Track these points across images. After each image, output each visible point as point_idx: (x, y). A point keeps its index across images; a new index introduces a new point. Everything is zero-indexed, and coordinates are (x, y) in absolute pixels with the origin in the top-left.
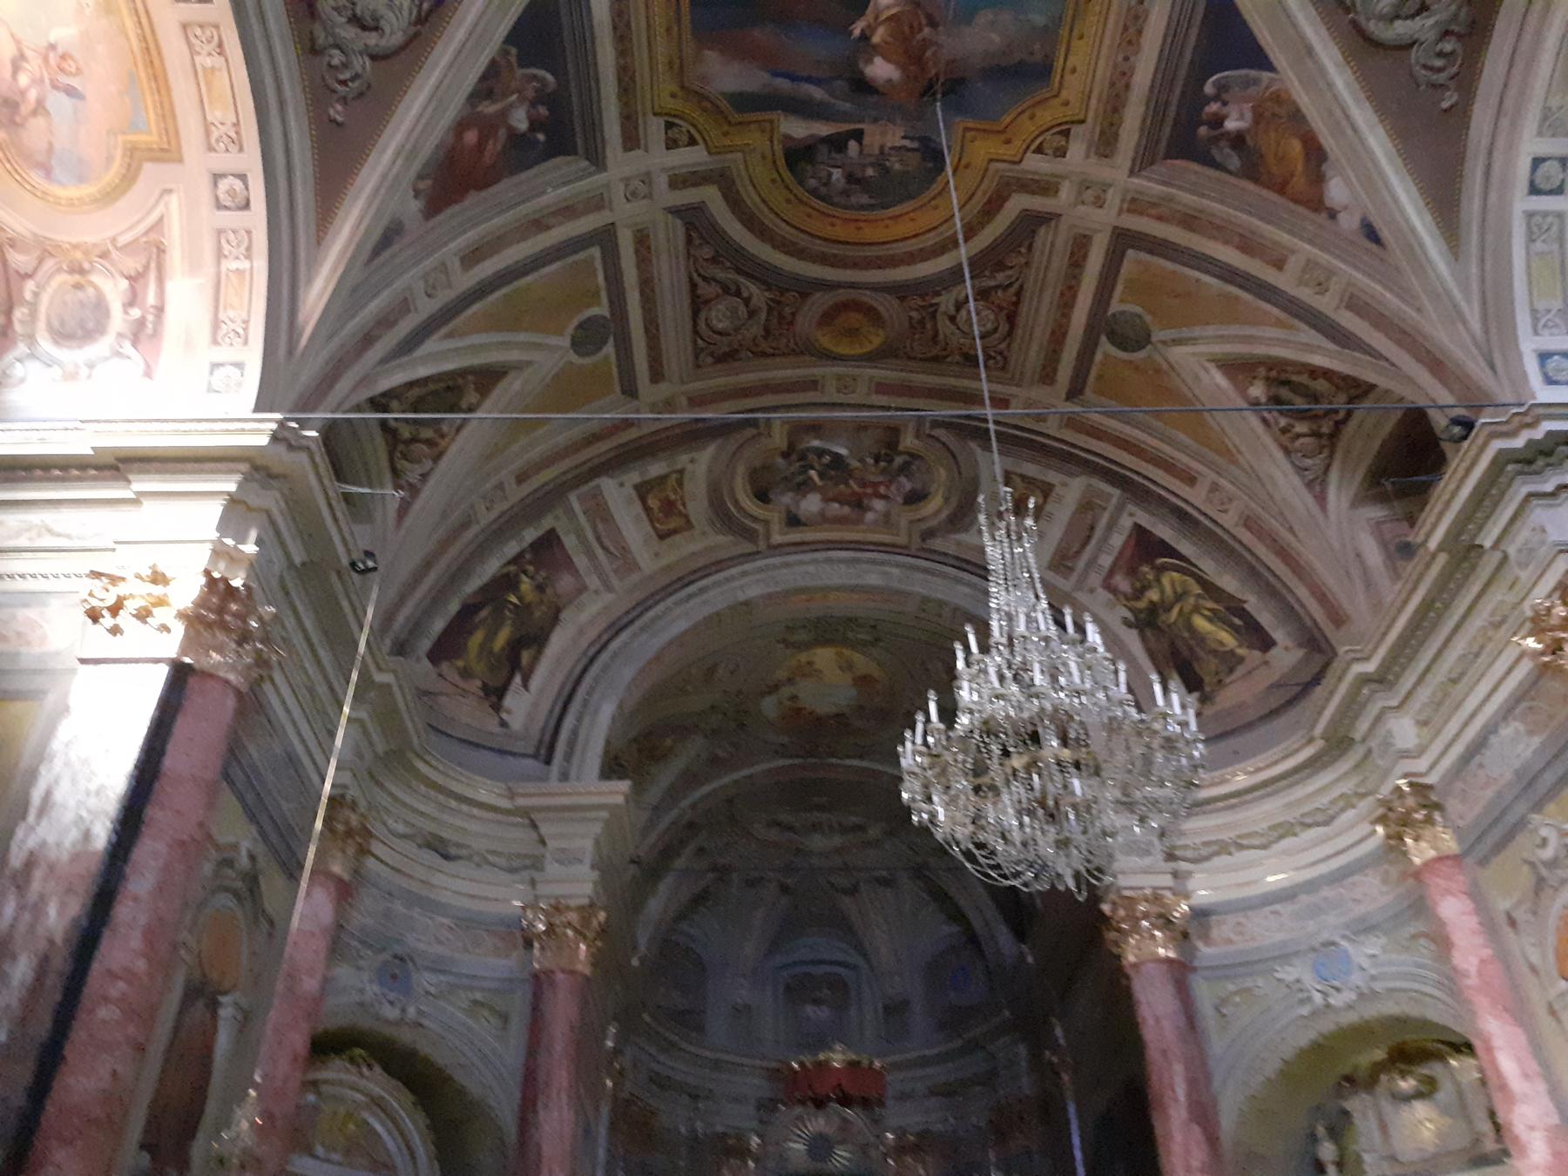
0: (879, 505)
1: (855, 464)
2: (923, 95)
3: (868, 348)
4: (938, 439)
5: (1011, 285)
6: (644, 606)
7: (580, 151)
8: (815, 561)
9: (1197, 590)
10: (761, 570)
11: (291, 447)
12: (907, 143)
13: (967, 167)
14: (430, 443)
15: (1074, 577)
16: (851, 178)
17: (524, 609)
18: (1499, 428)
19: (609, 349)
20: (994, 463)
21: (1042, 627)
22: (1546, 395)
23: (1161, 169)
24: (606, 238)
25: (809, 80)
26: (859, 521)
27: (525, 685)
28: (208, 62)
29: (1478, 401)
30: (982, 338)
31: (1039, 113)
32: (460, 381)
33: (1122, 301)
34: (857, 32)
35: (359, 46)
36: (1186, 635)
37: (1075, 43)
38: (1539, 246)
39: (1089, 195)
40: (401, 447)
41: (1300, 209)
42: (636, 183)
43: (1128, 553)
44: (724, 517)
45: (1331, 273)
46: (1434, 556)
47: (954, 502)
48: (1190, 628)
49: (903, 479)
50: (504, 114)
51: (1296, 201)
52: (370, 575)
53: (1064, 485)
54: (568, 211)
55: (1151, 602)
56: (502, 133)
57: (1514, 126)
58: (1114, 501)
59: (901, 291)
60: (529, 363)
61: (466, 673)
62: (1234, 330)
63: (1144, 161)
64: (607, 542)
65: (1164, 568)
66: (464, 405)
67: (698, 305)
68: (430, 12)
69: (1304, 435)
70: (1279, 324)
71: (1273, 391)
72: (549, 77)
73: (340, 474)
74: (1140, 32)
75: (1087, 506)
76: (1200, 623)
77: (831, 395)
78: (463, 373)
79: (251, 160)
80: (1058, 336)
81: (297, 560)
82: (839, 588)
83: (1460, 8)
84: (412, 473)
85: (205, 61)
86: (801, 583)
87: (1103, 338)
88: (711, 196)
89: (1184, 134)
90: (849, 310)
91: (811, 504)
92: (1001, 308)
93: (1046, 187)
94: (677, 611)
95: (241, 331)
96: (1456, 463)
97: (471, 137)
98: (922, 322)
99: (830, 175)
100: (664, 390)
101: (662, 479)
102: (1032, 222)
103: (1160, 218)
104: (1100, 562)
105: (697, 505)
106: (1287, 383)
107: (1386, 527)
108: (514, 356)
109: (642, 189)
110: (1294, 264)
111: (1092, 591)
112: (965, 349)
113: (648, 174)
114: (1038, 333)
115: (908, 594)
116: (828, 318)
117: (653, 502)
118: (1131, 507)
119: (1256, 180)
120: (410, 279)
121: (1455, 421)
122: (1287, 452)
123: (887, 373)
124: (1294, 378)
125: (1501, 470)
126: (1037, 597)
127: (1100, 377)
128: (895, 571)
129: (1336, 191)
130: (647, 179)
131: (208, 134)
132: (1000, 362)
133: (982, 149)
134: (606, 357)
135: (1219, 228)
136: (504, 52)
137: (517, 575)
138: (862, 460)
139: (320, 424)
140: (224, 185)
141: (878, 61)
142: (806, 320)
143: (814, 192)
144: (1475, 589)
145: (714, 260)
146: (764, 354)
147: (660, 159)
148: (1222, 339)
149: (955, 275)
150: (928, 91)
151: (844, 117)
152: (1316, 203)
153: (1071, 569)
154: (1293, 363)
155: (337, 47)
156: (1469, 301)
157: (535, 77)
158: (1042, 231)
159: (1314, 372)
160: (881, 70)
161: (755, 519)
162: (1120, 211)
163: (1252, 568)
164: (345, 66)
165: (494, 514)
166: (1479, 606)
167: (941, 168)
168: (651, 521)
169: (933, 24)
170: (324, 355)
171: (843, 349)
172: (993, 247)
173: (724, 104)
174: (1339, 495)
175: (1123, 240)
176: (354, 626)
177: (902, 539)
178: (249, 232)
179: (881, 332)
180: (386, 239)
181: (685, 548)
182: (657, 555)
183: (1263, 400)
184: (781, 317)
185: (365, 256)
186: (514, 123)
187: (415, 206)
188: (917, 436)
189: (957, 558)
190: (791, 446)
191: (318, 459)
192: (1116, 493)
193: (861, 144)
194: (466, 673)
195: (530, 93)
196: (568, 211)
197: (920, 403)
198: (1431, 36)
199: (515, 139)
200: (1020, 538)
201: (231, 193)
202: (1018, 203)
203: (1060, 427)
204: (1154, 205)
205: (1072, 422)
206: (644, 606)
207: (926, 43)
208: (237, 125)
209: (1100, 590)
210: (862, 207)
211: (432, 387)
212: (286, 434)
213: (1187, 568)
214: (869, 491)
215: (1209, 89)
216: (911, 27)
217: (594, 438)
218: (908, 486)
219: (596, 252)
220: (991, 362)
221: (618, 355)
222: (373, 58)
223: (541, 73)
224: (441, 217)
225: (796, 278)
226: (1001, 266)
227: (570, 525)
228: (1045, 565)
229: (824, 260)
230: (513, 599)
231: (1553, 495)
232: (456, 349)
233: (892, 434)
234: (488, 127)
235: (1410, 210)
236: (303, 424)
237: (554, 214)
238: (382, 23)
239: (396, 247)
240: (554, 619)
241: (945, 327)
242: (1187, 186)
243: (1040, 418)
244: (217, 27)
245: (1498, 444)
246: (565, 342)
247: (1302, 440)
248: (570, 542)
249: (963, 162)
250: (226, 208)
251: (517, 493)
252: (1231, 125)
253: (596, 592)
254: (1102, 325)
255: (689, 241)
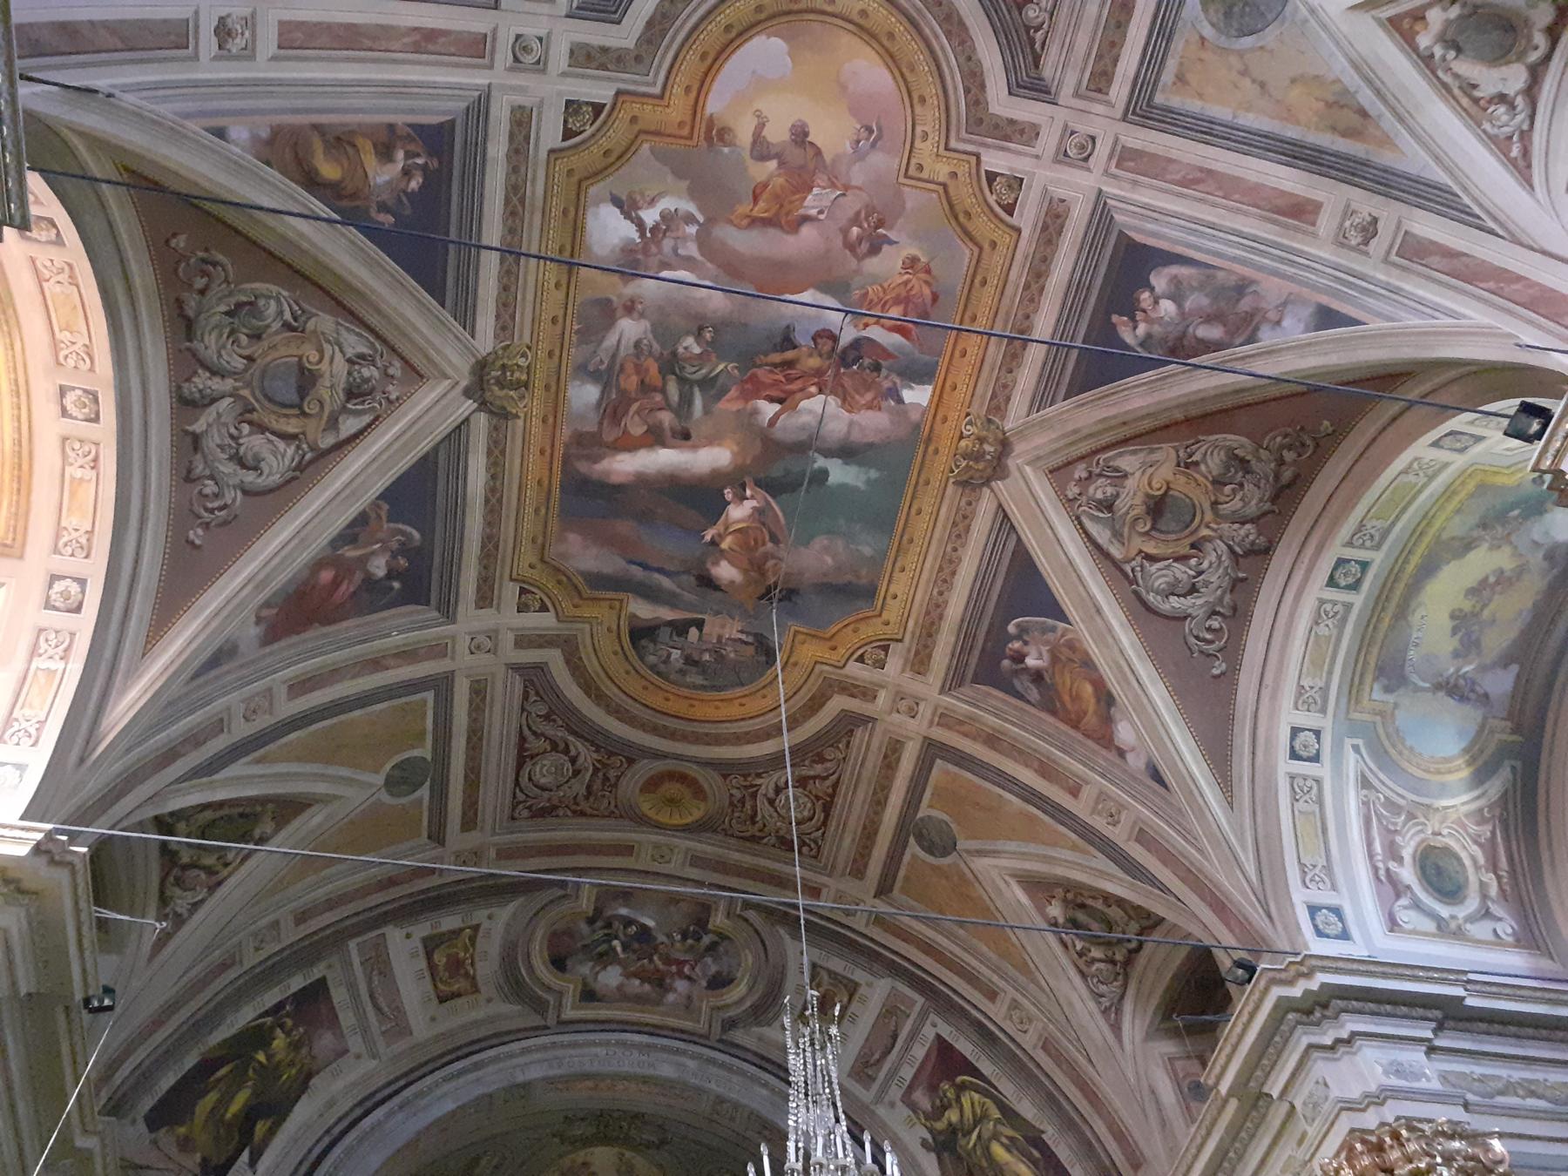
0: (681, 985)
1: (661, 938)
2: (761, 598)
3: (689, 820)
4: (746, 920)
5: (827, 778)
6: (410, 1077)
7: (433, 601)
8: (607, 1043)
9: (996, 1113)
10: (544, 1048)
11: (53, 862)
12: (743, 637)
13: (795, 664)
14: (210, 871)
15: (875, 1086)
16: (689, 661)
17: (270, 1072)
18: (1278, 976)
19: (424, 792)
20: (801, 955)
21: (841, 1154)
22: (1318, 947)
23: (966, 690)
24: (442, 685)
25: (660, 570)
26: (658, 1003)
27: (253, 1163)
28: (79, 473)
29: (1260, 946)
30: (798, 824)
31: (862, 626)
32: (259, 809)
33: (930, 806)
34: (708, 538)
35: (236, 481)
36: (985, 1164)
37: (896, 574)
38: (1300, 805)
39: (903, 705)
40: (176, 871)
41: (1090, 743)
42: (481, 638)
43: (929, 1067)
44: (515, 986)
45: (1122, 807)
46: (1225, 1101)
47: (760, 989)
48: (987, 1151)
49: (709, 960)
50: (363, 561)
51: (1088, 736)
52: (103, 1016)
53: (869, 985)
54: (408, 655)
55: (950, 1124)
56: (358, 577)
57: (1274, 697)
58: (917, 1008)
59: (725, 768)
60: (335, 797)
61: (185, 1144)
62: (1032, 848)
63: (954, 681)
64: (381, 1001)
65: (962, 1088)
66: (257, 833)
67: (523, 757)
68: (311, 462)
69: (1100, 961)
70: (1074, 848)
71: (1070, 913)
72: (416, 535)
73: (100, 899)
74: (954, 573)
75: (891, 1012)
76: (998, 1150)
77: (643, 862)
78: (263, 801)
79: (96, 569)
80: (869, 833)
81: (23, 991)
82: (626, 1077)
83: (1224, 593)
84: (181, 902)
85: (74, 472)
86: (588, 1068)
87: (912, 840)
88: (554, 659)
89: (988, 663)
90: (675, 780)
91: (611, 977)
92: (818, 798)
93: (868, 693)
94: (446, 1087)
95: (33, 731)
96: (1242, 1001)
97: (326, 576)
98: (742, 801)
99: (669, 655)
100: (473, 839)
101: (456, 933)
102: (849, 723)
103: (966, 735)
104: (901, 1074)
105: (487, 968)
106: (1082, 906)
107: (1179, 1064)
108: (321, 788)
109: (489, 644)
110: (1087, 793)
111: (892, 1105)
112: (781, 833)
113: (496, 631)
114: (852, 824)
115: (700, 1091)
116: (652, 784)
117: (440, 958)
118: (933, 1017)
119: (1054, 713)
120: (233, 700)
121: (1239, 964)
122: (1083, 975)
123: (706, 847)
124: (1090, 902)
125: (1281, 1020)
126: (837, 1121)
127: (907, 878)
128: (691, 1064)
129: (1124, 733)
130: (493, 635)
131: (58, 537)
132: (813, 850)
133: (809, 652)
134: (420, 801)
135: (1021, 752)
136: (375, 505)
137: (272, 1028)
138: (669, 936)
139: (91, 841)
140: (59, 586)
141: (724, 563)
142: (630, 784)
143: (652, 668)
144: (1266, 1141)
145: (547, 717)
146: (583, 814)
147: (508, 618)
148: (1024, 856)
149: (776, 761)
150: (767, 594)
151: (690, 607)
152: (1105, 738)
153: (873, 1079)
154: (1091, 888)
155: (212, 477)
156: (1244, 848)
157: (403, 533)
158: (859, 733)
159: (1108, 898)
160: (725, 572)
161: (549, 989)
162: (931, 723)
163: (1050, 1096)
164: (216, 496)
165: (263, 954)
166: (1271, 1161)
167: (771, 661)
168: (434, 979)
169: (774, 539)
170: (118, 767)
171: (663, 818)
172: (818, 737)
173: (579, 581)
174: (1134, 1024)
175: (932, 751)
176: (69, 1079)
177: (701, 1027)
178: (72, 635)
179: (702, 805)
180: (216, 659)
181: (467, 1015)
182: (433, 1019)
183: (1061, 920)
184: (606, 779)
185: (185, 676)
186: (372, 569)
187: (254, 631)
188: (728, 916)
189: (756, 1054)
190: (598, 911)
191: (80, 880)
192: (920, 1000)
193: (701, 631)
194: (185, 1144)
195: (394, 545)
196: (408, 655)
197: (733, 882)
198: (1201, 613)
199: (370, 583)
200: (823, 1048)
201: (65, 595)
202: (838, 703)
203: (867, 925)
204: (961, 723)
205: (879, 920)
206: (410, 1077)
207: (766, 557)
208: (91, 533)
209: (900, 1104)
210: (695, 687)
211: (226, 811)
212: (51, 846)
213: (988, 1090)
214: (674, 969)
215: (1011, 628)
216: (756, 540)
217: (392, 882)
218: (713, 969)
219: (429, 696)
220: (805, 849)
221: (432, 797)
222: (245, 492)
223: (409, 529)
224: (276, 646)
225: (629, 745)
226: (821, 759)
227: (345, 979)
228: (848, 1068)
229: (655, 730)
230: (261, 1057)
231: (1332, 1048)
232: (262, 776)
233: (703, 911)
234: (344, 570)
235: (1188, 758)
236: (74, 837)
237: (396, 655)
238: (263, 464)
239: (225, 668)
240: (303, 1084)
241: (762, 804)
242: (991, 709)
243: (848, 913)
244: (97, 444)
245: (1277, 992)
246: (379, 779)
247: (1097, 965)
248: (339, 995)
249: (792, 660)
250: (57, 609)
251: (291, 935)
252: (1031, 662)
253: (358, 1057)
254: (908, 826)
255: (526, 697)
